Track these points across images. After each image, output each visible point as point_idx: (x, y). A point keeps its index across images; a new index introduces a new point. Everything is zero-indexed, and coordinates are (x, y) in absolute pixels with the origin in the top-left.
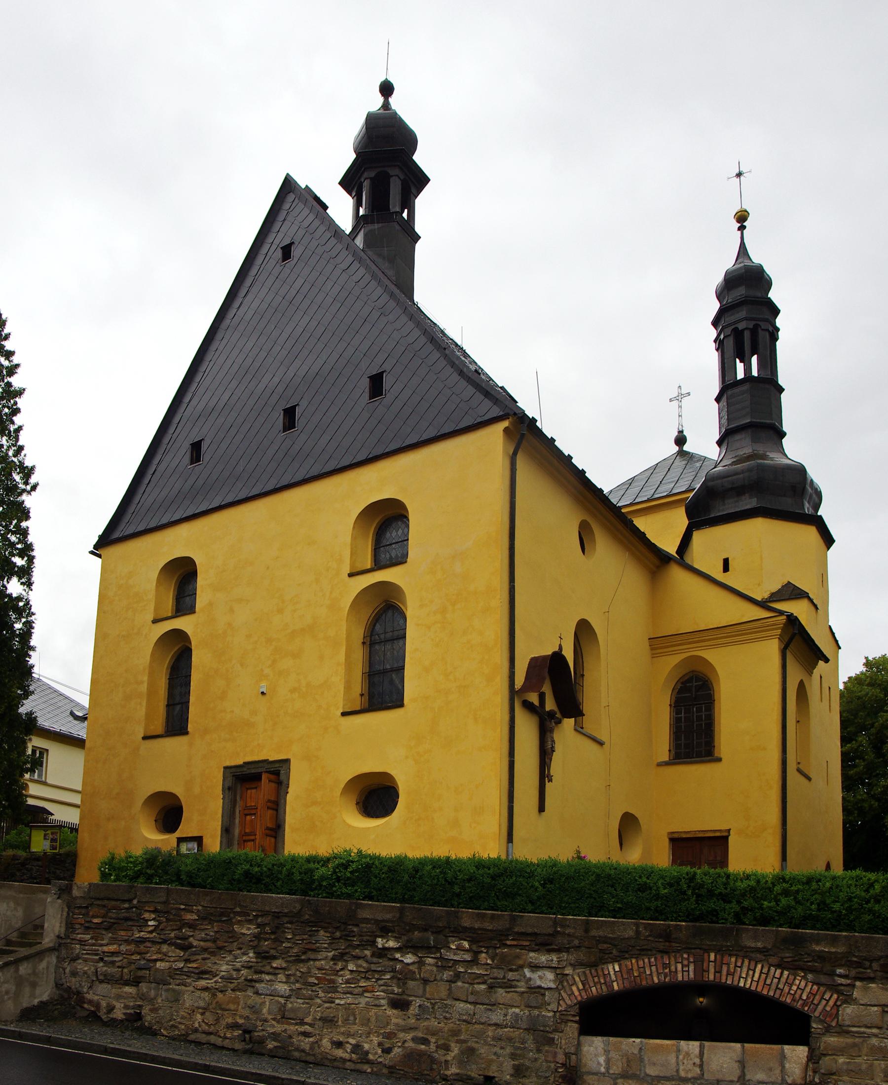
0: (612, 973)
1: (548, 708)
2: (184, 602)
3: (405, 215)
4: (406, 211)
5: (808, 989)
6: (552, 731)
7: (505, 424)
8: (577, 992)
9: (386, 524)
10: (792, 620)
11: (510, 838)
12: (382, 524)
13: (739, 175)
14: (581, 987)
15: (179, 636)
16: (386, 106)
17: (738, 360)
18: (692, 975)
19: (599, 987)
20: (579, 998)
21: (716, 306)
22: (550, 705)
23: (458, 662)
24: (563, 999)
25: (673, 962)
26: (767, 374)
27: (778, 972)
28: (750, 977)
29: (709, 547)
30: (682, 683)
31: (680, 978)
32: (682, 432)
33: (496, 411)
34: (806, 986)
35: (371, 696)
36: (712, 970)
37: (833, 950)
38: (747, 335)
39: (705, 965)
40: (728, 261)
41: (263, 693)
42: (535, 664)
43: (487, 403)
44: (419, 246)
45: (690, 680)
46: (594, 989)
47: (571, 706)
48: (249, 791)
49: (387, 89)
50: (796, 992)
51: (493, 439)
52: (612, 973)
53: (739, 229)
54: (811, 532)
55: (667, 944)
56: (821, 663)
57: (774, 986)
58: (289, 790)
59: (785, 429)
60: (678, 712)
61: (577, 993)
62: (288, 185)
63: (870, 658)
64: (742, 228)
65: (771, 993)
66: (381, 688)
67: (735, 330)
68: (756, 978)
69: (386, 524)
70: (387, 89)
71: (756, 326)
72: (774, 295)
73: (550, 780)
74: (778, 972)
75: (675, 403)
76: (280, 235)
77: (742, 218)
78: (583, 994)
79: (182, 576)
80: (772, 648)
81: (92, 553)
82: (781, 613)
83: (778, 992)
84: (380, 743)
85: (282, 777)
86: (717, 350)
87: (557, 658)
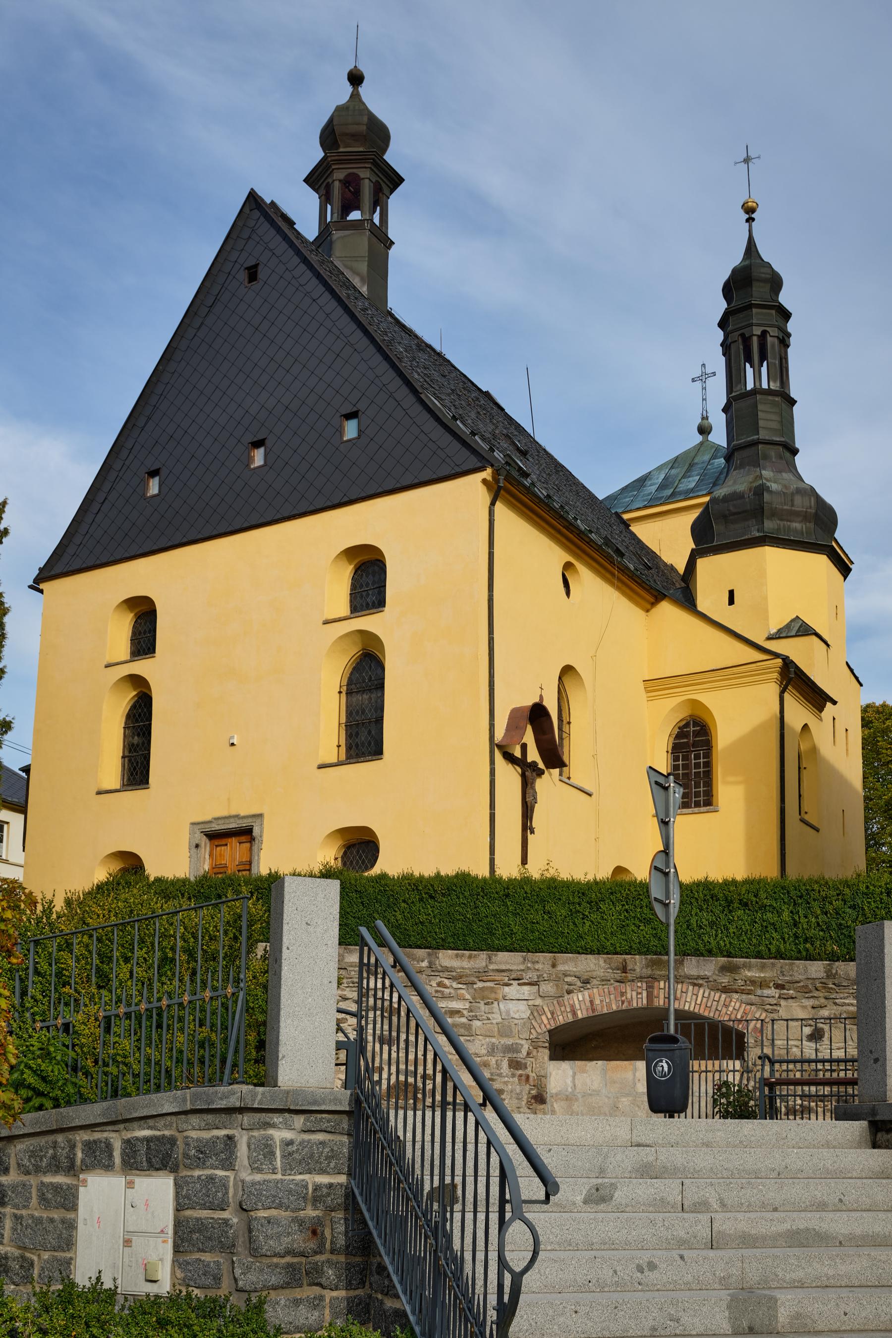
0: (576, 1002)
1: (529, 760)
2: (144, 642)
3: (376, 219)
4: (378, 208)
6: (533, 783)
7: (487, 474)
8: (546, 1023)
9: (369, 578)
11: (524, 861)
13: (747, 160)
14: (549, 1016)
15: (138, 682)
16: (355, 96)
17: (748, 365)
18: (645, 1002)
19: (565, 1015)
20: (548, 1027)
21: (722, 305)
22: (533, 755)
23: (439, 718)
24: (534, 1028)
25: (629, 991)
26: (775, 386)
27: (718, 995)
28: (693, 1000)
29: (715, 574)
30: (679, 728)
31: (635, 1005)
32: (707, 418)
34: (740, 1007)
35: (349, 748)
36: (662, 996)
37: (762, 975)
40: (736, 257)
41: (233, 744)
42: (515, 715)
43: (465, 453)
44: (392, 252)
45: (687, 725)
46: (561, 1017)
47: (554, 757)
48: (218, 849)
49: (356, 78)
51: (472, 490)
52: (576, 1002)
53: (747, 221)
54: (822, 561)
55: (624, 974)
56: (829, 704)
57: (714, 1008)
58: (263, 846)
59: (797, 446)
60: (676, 759)
61: (546, 1022)
62: (253, 198)
63: (443, 873)
64: (750, 220)
65: (712, 1015)
66: (364, 737)
67: (742, 335)
68: (698, 1002)
69: (369, 578)
70: (356, 78)
71: (764, 333)
72: (785, 298)
73: (532, 832)
74: (718, 995)
75: (698, 384)
77: (750, 211)
78: (552, 1022)
79: (144, 616)
80: (773, 689)
81: (30, 587)
82: (776, 655)
83: (717, 1013)
84: (361, 796)
85: (256, 832)
87: (537, 714)
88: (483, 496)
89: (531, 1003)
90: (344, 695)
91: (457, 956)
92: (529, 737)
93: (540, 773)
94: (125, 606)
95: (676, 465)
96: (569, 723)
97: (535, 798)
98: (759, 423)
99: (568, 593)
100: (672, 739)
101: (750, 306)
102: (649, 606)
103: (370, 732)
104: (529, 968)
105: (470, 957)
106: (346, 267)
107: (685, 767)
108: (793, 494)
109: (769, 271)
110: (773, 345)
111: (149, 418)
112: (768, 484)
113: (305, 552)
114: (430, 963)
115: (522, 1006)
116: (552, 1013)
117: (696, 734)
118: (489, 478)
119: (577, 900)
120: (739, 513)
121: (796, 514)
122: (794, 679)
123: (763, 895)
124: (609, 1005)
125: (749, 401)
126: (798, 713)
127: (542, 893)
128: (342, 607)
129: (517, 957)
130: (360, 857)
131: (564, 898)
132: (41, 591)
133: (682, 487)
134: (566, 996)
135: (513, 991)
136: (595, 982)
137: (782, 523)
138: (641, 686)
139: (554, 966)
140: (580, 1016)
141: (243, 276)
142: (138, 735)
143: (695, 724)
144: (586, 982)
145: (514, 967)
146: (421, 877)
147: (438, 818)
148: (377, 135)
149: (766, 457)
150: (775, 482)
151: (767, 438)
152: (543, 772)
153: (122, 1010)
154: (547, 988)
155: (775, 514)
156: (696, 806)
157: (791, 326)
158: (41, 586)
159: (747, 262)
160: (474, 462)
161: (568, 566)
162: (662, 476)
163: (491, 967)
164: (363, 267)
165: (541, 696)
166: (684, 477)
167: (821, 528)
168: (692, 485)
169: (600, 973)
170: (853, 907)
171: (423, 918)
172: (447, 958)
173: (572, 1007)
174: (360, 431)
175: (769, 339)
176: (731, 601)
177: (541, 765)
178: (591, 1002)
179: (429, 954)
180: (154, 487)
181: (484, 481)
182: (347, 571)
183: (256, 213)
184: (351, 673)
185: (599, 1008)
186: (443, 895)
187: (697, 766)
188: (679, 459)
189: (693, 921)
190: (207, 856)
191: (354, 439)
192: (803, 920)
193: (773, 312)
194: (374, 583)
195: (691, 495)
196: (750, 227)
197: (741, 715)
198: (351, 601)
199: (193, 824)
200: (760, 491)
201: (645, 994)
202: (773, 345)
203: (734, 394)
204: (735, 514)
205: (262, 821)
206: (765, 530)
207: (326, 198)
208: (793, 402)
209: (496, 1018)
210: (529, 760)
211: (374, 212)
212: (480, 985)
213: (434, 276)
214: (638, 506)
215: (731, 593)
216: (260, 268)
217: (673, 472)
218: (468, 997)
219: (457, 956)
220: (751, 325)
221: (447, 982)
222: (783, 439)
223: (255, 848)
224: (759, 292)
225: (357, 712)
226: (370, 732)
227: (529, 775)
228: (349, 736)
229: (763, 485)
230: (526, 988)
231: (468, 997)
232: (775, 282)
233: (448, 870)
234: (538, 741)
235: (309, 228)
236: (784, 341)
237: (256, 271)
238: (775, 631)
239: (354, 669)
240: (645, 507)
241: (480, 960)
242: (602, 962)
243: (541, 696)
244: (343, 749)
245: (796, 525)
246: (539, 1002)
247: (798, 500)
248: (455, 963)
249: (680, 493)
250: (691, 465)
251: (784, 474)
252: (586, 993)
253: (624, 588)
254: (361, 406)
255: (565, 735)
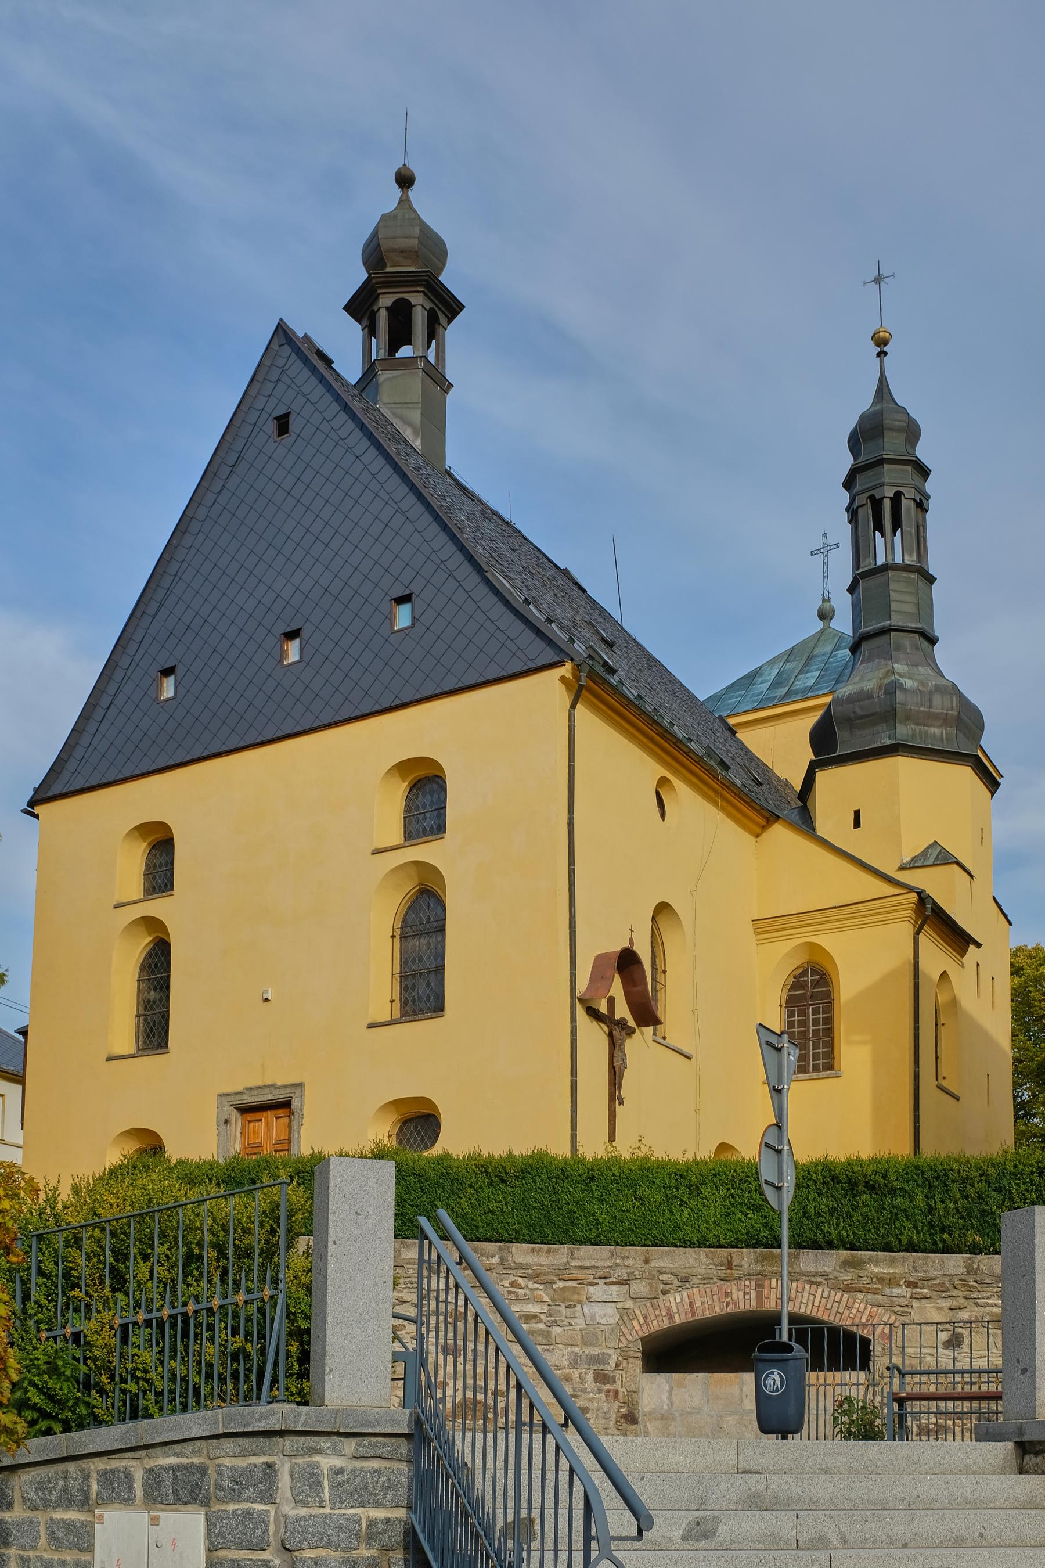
0: (673, 1305)
1: (617, 1017)
2: (160, 877)
5: (867, 1312)
7: (566, 670)
8: (637, 1331)
9: (426, 793)
10: (923, 899)
11: (612, 1138)
12: (414, 786)
13: (878, 280)
14: (642, 1321)
15: (151, 923)
16: (404, 202)
18: (753, 1303)
21: (848, 461)
22: (622, 1011)
25: (735, 1291)
26: (910, 560)
27: (839, 1295)
30: (795, 977)
33: (550, 656)
35: (404, 1003)
36: (773, 1297)
38: (887, 505)
39: (766, 1291)
40: (864, 402)
41: (267, 1000)
43: (539, 644)
45: (804, 973)
46: (655, 1322)
47: (646, 1014)
49: (405, 180)
50: (855, 1316)
51: (549, 689)
52: (673, 1305)
53: (878, 355)
54: (965, 773)
56: (972, 947)
59: (936, 633)
60: (791, 1014)
61: (637, 1328)
63: (516, 1153)
64: (882, 354)
65: (832, 1318)
66: (421, 991)
67: (872, 498)
68: (817, 1303)
69: (426, 793)
70: (405, 180)
71: (898, 494)
73: (621, 1103)
74: (839, 1295)
75: (819, 558)
76: (273, 401)
77: (881, 342)
78: (645, 1328)
80: (905, 929)
82: (910, 889)
83: (839, 1316)
84: (420, 1061)
85: (295, 1104)
86: (850, 522)
87: (627, 961)
88: (561, 697)
89: (620, 1305)
90: (397, 940)
91: (533, 1250)
92: (617, 988)
93: (631, 1032)
94: (136, 834)
95: (792, 658)
96: (664, 972)
97: (625, 1063)
98: (888, 608)
99: (663, 815)
100: (786, 991)
101: (881, 462)
102: (759, 830)
103: (428, 984)
104: (617, 1265)
105: (548, 1252)
106: (395, 415)
107: (802, 1023)
108: (931, 692)
109: (904, 417)
110: (908, 510)
111: (161, 604)
112: (902, 680)
113: (352, 764)
114: (501, 1258)
115: (610, 1309)
116: (645, 1318)
117: (815, 984)
118: (569, 676)
119: (674, 1183)
120: (867, 716)
121: (936, 716)
122: (934, 918)
123: (892, 1176)
124: (711, 1307)
125: (879, 579)
126: (935, 957)
127: (633, 1176)
128: (396, 836)
129: (605, 1250)
130: (419, 1133)
131: (658, 1181)
132: (37, 816)
133: (799, 685)
134: (662, 1298)
135: (598, 1291)
136: (695, 1280)
137: (918, 728)
138: (750, 927)
139: (647, 1262)
140: (677, 1320)
141: (272, 427)
142: (155, 989)
143: (814, 972)
144: (685, 1280)
145: (600, 1264)
146: (491, 1157)
147: (512, 1089)
148: (431, 250)
149: (898, 648)
150: (910, 678)
151: (900, 624)
152: (634, 1032)
153: (142, 1316)
154: (639, 1288)
155: (908, 718)
156: (814, 1071)
157: (930, 486)
158: (37, 810)
159: (878, 407)
160: (550, 656)
161: (663, 782)
162: (775, 672)
163: (573, 1263)
164: (416, 416)
165: (631, 940)
166: (801, 672)
167: (964, 734)
168: (811, 682)
169: (701, 1270)
170: (998, 1190)
171: (493, 1205)
172: (521, 1253)
173: (669, 1309)
174: (413, 618)
175: (904, 502)
176: (857, 824)
177: (631, 1023)
178: (691, 1304)
179: (500, 1249)
180: (168, 688)
181: (563, 679)
182: (401, 788)
183: (287, 350)
184: (407, 913)
185: (700, 1311)
186: (517, 1178)
187: (816, 1022)
188: (796, 651)
189: (811, 1208)
190: (238, 1134)
191: (406, 628)
192: (940, 1206)
193: (909, 468)
194: (432, 803)
195: (810, 694)
196: (882, 362)
197: (869, 960)
198: (405, 826)
199: (220, 1095)
200: (892, 689)
201: (753, 1294)
202: (908, 510)
203: (861, 570)
204: (862, 717)
205: (302, 1091)
206: (898, 736)
207: (371, 330)
208: (931, 580)
209: (580, 1323)
210: (617, 1017)
211: (429, 347)
212: (560, 1284)
213: (499, 426)
214: (746, 709)
215: (857, 814)
216: (292, 418)
217: (788, 666)
218: (546, 1298)
219: (533, 1250)
220: (882, 485)
221: (521, 1281)
222: (919, 626)
223: (295, 1124)
224: (892, 445)
225: (414, 961)
226: (428, 984)
227: (616, 1032)
228: (404, 989)
229: (895, 681)
230: (615, 1288)
231: (546, 1298)
232: (912, 432)
233: (522, 1148)
234: (628, 992)
235: (350, 367)
236: (921, 506)
237: (287, 422)
238: (909, 859)
239: (409, 908)
240: (756, 710)
241: (561, 1255)
242: (703, 1257)
243: (631, 940)
244: (397, 1005)
245: (935, 731)
246: (629, 1304)
247: (937, 700)
248: (531, 1259)
249: (797, 692)
250: (810, 658)
251: (920, 668)
252: (685, 1293)
253: (730, 808)
254: (415, 588)
255: (659, 987)
